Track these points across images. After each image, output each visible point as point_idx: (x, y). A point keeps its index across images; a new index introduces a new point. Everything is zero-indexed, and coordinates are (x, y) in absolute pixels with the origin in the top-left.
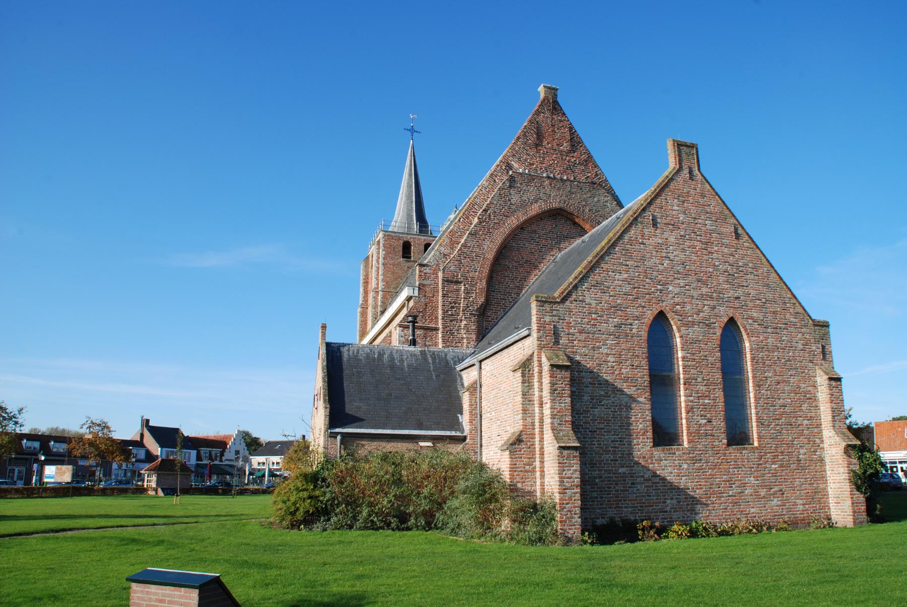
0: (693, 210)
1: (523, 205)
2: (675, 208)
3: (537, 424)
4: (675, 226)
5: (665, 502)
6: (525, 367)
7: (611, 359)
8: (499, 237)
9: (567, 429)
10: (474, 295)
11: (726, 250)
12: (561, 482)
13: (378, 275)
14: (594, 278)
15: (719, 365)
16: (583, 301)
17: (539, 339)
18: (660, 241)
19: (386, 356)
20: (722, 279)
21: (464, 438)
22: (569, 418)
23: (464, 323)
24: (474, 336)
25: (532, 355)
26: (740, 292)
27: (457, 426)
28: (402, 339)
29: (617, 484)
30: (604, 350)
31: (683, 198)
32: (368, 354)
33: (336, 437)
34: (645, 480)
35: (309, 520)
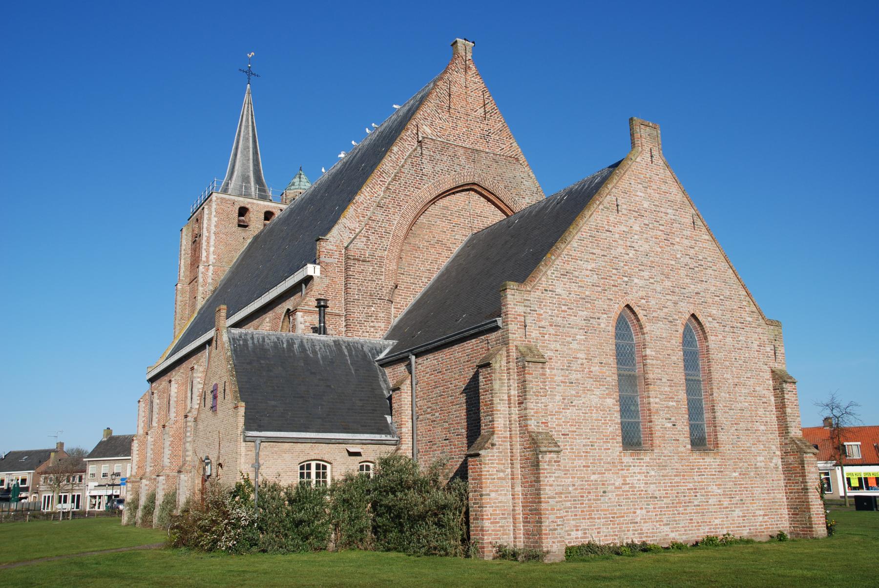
5: (635, 513)
7: (581, 355)
10: (382, 277)
12: (804, 476)
19: (296, 346)
20: (683, 272)
26: (700, 287)
29: (589, 493)
30: (574, 345)
32: (275, 343)
34: (616, 488)
35: (176, 546)
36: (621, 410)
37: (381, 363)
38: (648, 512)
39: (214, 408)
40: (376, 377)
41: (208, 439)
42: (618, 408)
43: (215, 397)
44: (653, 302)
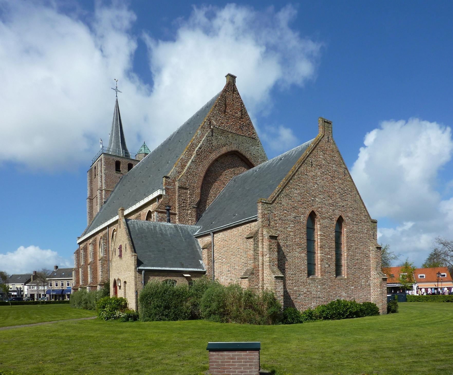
0: (328, 158)
1: (219, 147)
2: (321, 157)
3: (260, 265)
4: (321, 166)
6: (253, 237)
7: (291, 234)
8: (206, 164)
9: (276, 268)
10: (194, 196)
11: (340, 181)
13: (102, 180)
14: (286, 191)
15: (334, 239)
16: (281, 203)
18: (314, 174)
20: (338, 196)
21: (205, 273)
22: (276, 263)
24: (194, 219)
25: (258, 230)
26: (344, 203)
27: (199, 266)
28: (158, 218)
31: (324, 151)
36: (307, 259)
37: (196, 236)
39: (120, 256)
40: (194, 243)
41: (118, 270)
42: (306, 258)
43: (121, 251)
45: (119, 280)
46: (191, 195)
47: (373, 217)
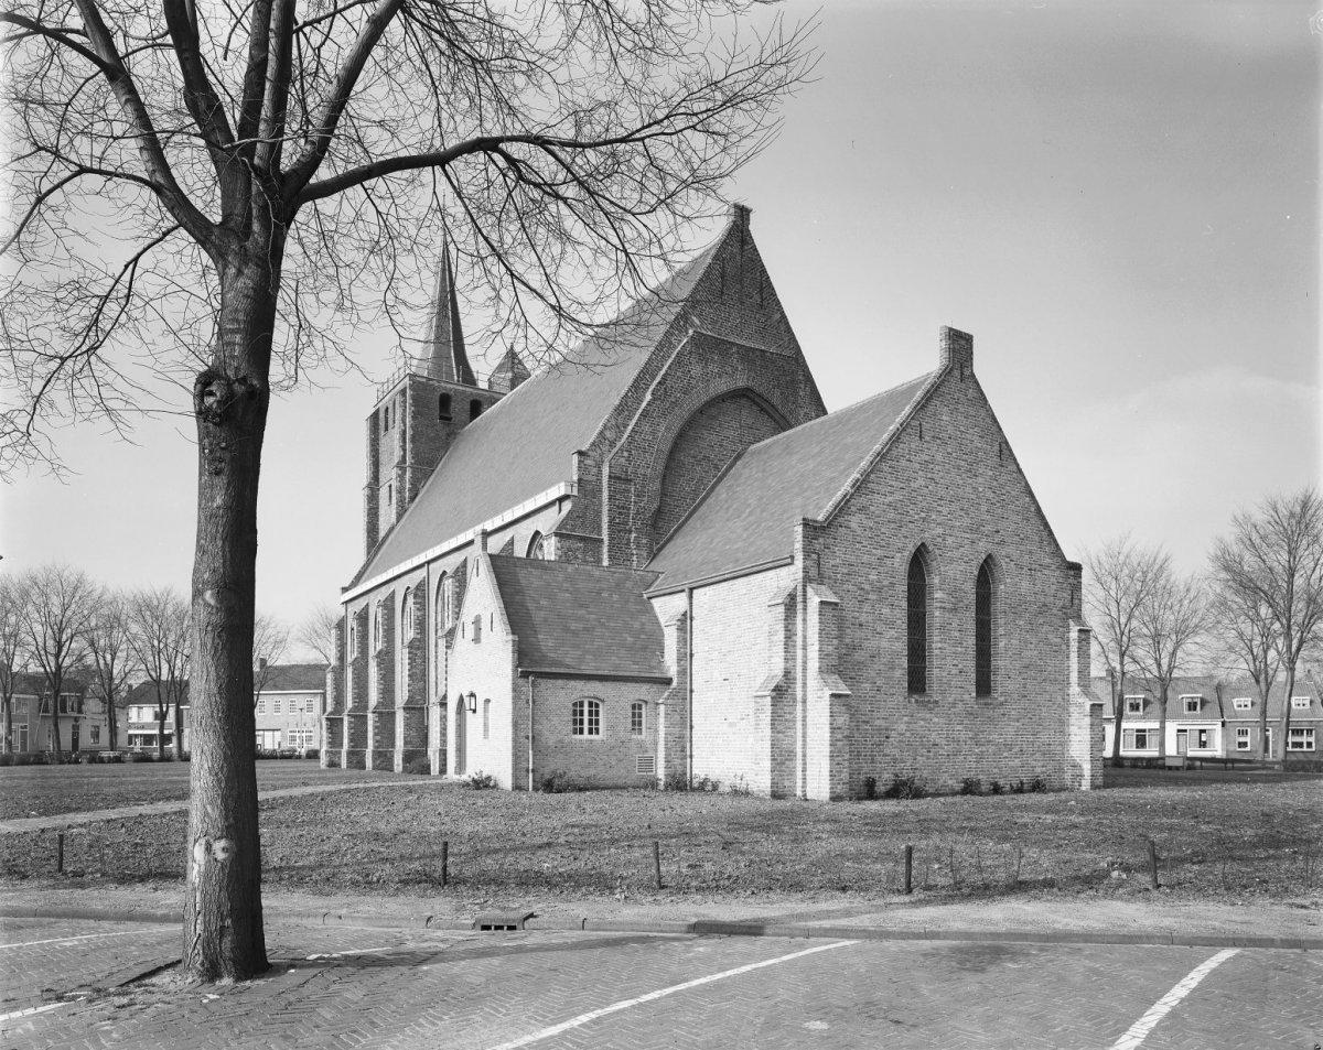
10: (646, 499)
17: (805, 570)
18: (927, 458)
23: (633, 535)
25: (795, 588)
33: (528, 677)
38: (928, 759)
39: (477, 640)
43: (478, 630)
44: (950, 540)
45: (472, 695)
46: (638, 496)
47: (1070, 558)
